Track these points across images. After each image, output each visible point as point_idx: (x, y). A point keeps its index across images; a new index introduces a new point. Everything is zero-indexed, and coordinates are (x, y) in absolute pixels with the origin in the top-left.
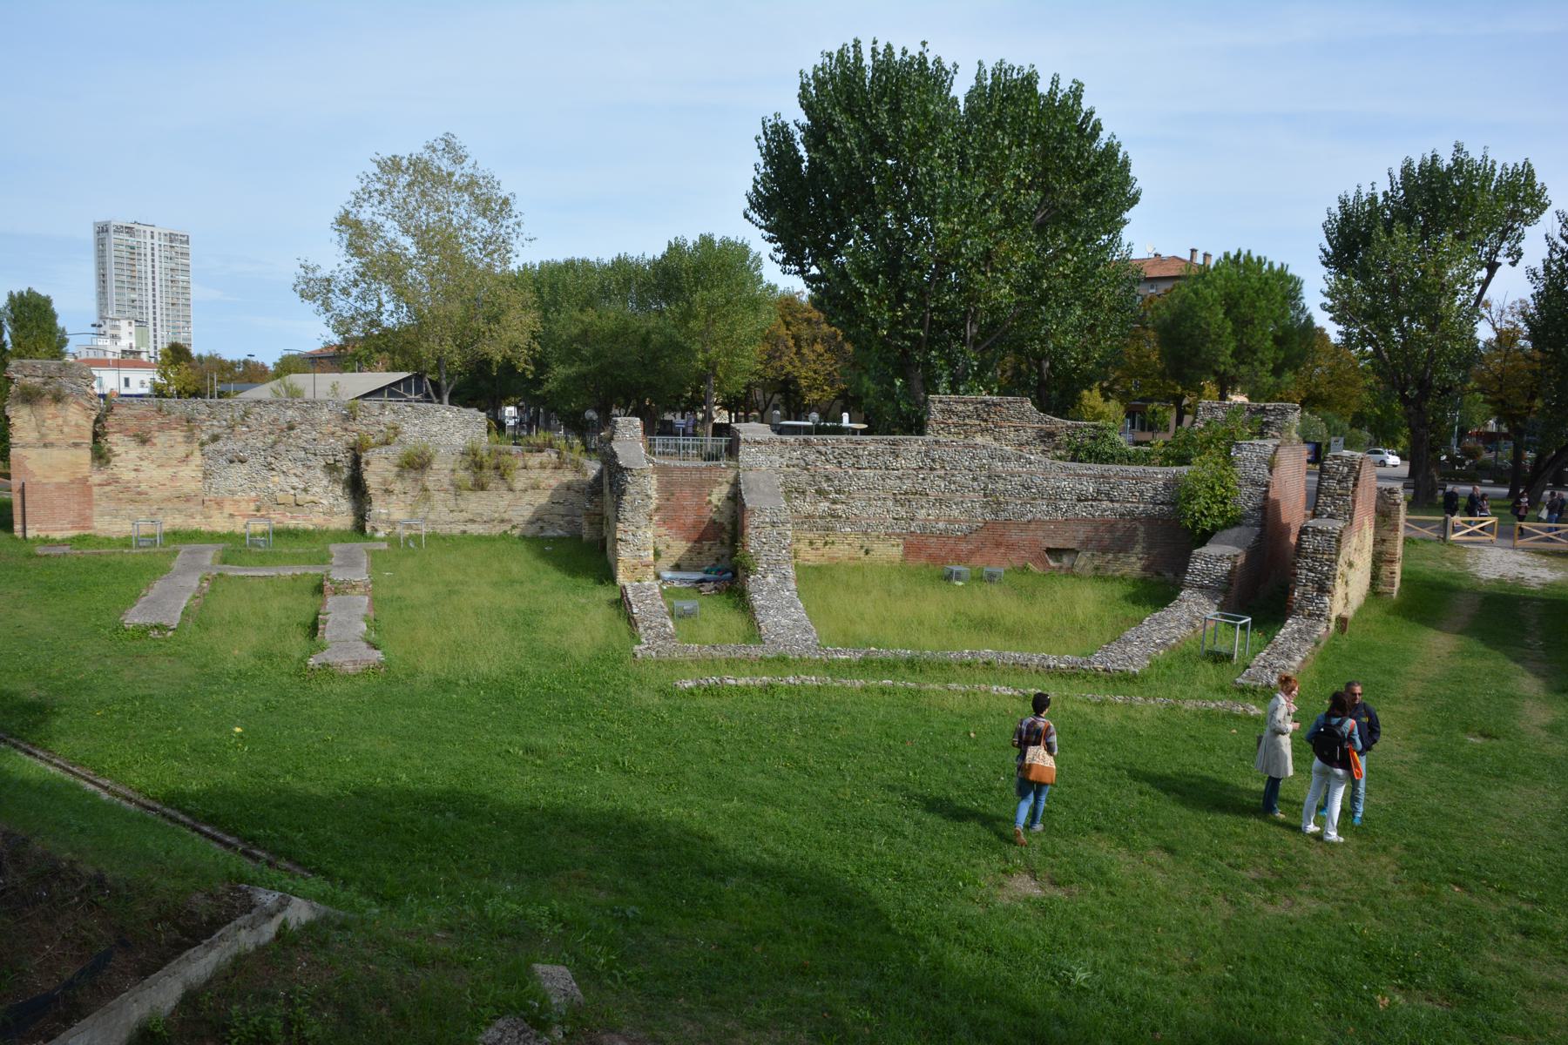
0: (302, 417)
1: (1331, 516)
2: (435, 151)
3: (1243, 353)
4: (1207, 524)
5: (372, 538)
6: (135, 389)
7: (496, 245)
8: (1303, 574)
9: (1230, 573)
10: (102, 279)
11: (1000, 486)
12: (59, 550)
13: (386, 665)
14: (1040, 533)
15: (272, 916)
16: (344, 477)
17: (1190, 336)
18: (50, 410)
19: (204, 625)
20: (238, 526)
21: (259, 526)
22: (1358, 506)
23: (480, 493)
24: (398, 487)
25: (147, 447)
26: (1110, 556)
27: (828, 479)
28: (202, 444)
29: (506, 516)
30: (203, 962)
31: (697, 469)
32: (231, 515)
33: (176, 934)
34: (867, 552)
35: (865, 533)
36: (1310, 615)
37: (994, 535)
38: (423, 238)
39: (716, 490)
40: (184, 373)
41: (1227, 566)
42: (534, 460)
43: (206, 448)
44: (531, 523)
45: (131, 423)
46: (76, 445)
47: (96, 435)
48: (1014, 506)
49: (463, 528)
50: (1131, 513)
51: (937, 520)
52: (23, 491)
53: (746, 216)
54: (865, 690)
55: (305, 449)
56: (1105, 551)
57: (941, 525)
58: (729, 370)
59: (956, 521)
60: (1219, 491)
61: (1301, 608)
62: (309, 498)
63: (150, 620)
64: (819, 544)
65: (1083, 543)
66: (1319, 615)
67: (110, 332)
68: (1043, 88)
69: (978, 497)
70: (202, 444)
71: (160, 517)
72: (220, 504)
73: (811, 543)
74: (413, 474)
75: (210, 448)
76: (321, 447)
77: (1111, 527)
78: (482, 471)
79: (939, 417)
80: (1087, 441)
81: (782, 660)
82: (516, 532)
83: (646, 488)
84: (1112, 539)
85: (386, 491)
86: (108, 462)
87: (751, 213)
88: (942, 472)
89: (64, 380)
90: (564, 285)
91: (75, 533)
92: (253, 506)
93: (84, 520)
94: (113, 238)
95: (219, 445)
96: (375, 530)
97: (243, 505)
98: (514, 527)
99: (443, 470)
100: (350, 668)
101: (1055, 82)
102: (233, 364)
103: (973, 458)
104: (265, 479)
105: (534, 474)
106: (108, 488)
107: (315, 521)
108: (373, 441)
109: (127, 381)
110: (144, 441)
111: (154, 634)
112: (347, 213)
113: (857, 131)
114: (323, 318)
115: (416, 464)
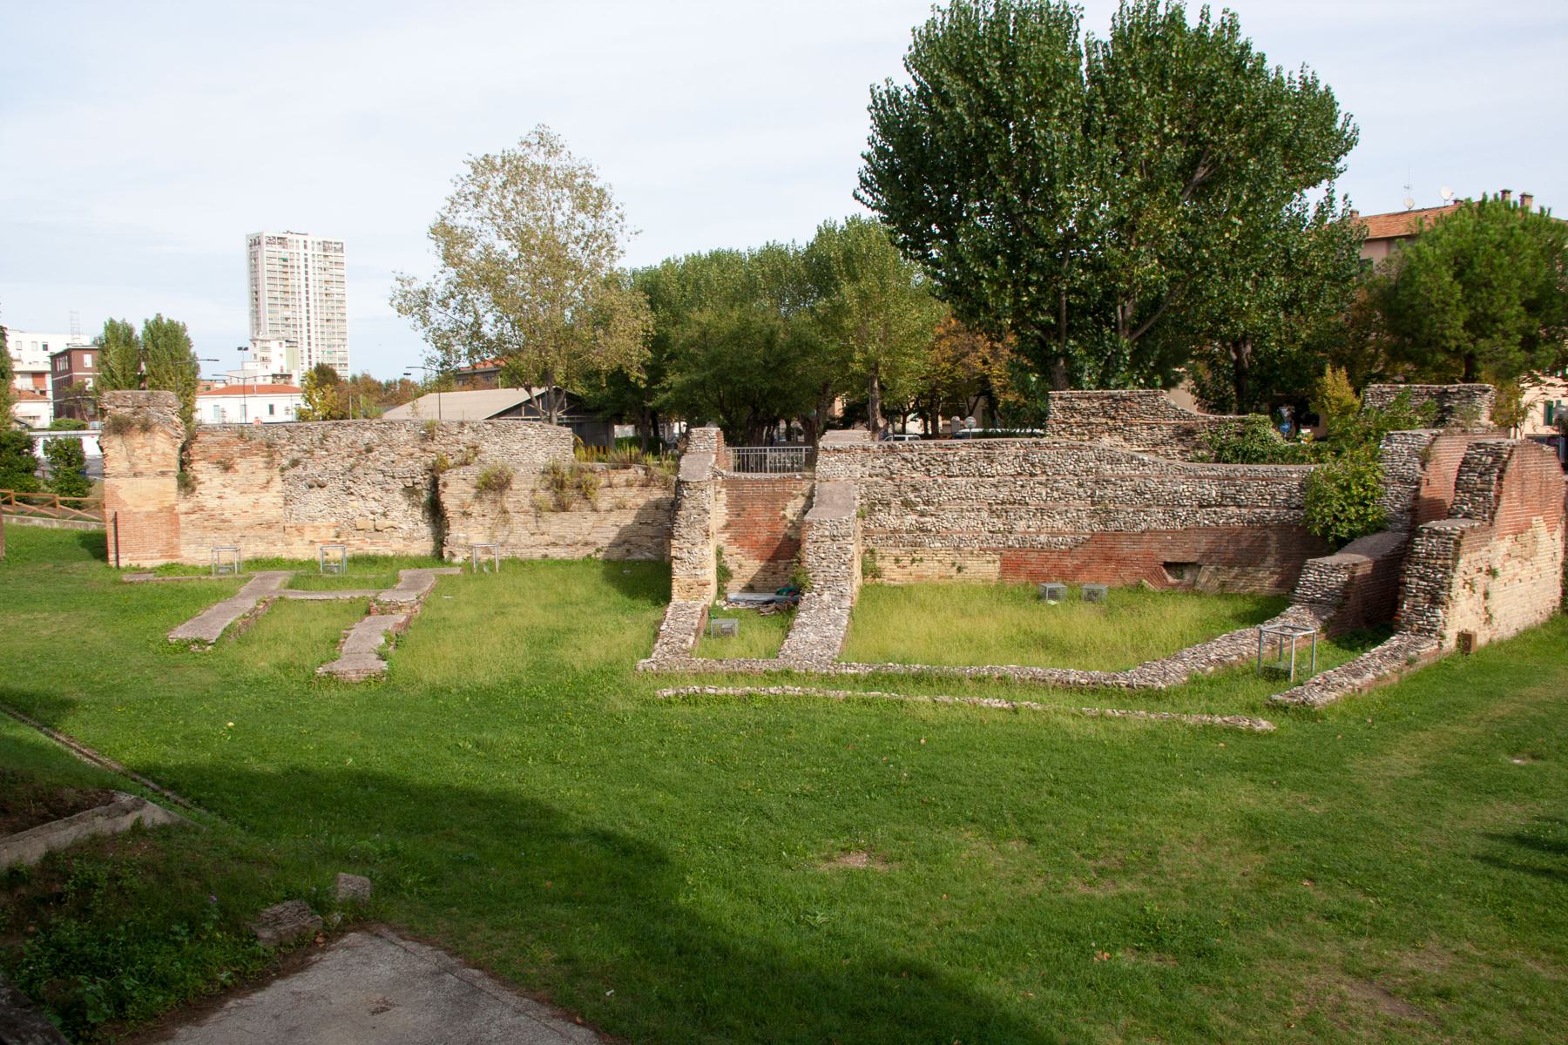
0: (380, 438)
1: (1467, 516)
2: (529, 145)
3: (1479, 325)
4: (1343, 530)
5: (449, 563)
6: (280, 416)
7: (601, 242)
8: (1413, 583)
9: (1347, 584)
10: (256, 296)
11: (1109, 492)
12: (143, 578)
13: (389, 675)
14: (1156, 545)
15: (128, 812)
16: (423, 500)
17: (1411, 307)
18: (138, 439)
19: (244, 642)
20: (315, 553)
21: (336, 554)
22: (1504, 502)
23: (563, 514)
24: (476, 509)
25: (230, 474)
26: (1236, 570)
27: (915, 489)
28: (283, 470)
29: (590, 539)
30: (64, 833)
31: (769, 481)
32: (312, 542)
33: (45, 811)
34: (959, 570)
35: (957, 548)
36: (1420, 631)
37: (1103, 549)
38: (523, 238)
39: (791, 504)
40: (330, 396)
41: (1344, 577)
42: (620, 477)
43: (287, 473)
44: (614, 545)
45: (214, 450)
46: (163, 473)
47: (183, 463)
48: (1125, 516)
49: (545, 551)
50: (1260, 519)
51: (1038, 533)
52: (115, 520)
53: (857, 198)
54: (848, 700)
55: (383, 472)
56: (1230, 564)
57: (1043, 538)
58: (893, 370)
59: (1060, 533)
60: (1356, 490)
61: (1410, 622)
62: (388, 523)
63: (191, 635)
64: (906, 561)
65: (1203, 555)
66: (1429, 631)
67: (261, 354)
68: (1192, 22)
69: (1085, 505)
70: (283, 470)
71: (242, 545)
72: (300, 530)
73: (897, 561)
74: (491, 496)
75: (290, 473)
76: (399, 469)
77: (1234, 535)
78: (564, 490)
79: (1060, 416)
80: (1233, 438)
81: (787, 674)
82: (600, 555)
83: (712, 508)
84: (1240, 551)
85: (464, 514)
86: (194, 490)
87: (861, 193)
88: (1044, 478)
89: (152, 410)
90: (707, 281)
91: (163, 562)
92: (332, 532)
93: (171, 548)
94: (265, 251)
95: (299, 470)
96: (453, 555)
97: (323, 532)
98: (598, 550)
99: (523, 490)
100: (353, 675)
101: (1205, 15)
102: (390, 385)
103: (1078, 461)
104: (344, 504)
105: (619, 493)
106: (193, 517)
107: (395, 547)
108: (450, 462)
109: (271, 408)
110: (227, 467)
111: (194, 648)
112: (444, 218)
113: (967, 92)
114: (422, 333)
115: (494, 485)
